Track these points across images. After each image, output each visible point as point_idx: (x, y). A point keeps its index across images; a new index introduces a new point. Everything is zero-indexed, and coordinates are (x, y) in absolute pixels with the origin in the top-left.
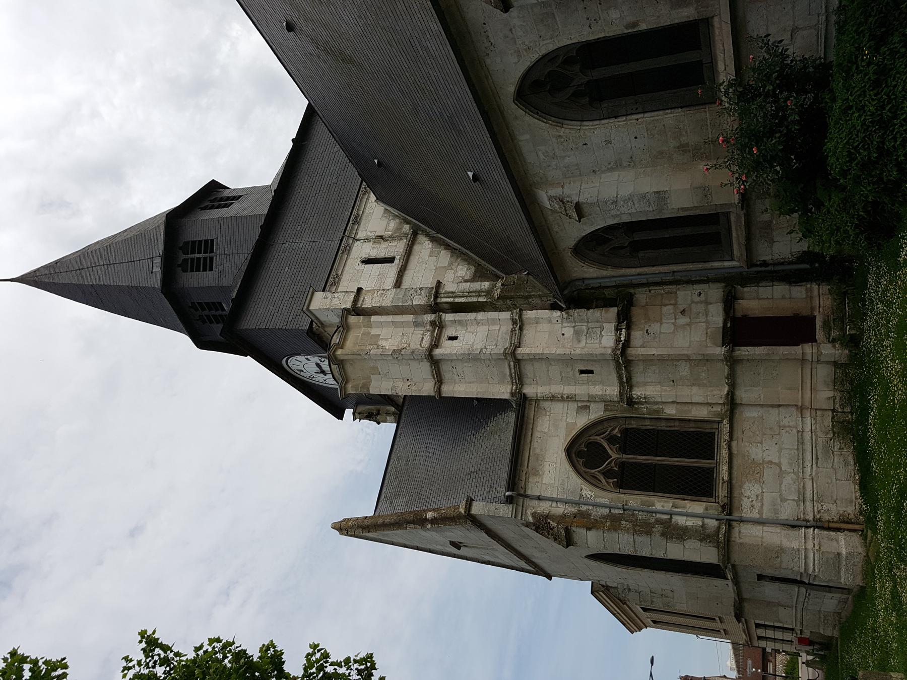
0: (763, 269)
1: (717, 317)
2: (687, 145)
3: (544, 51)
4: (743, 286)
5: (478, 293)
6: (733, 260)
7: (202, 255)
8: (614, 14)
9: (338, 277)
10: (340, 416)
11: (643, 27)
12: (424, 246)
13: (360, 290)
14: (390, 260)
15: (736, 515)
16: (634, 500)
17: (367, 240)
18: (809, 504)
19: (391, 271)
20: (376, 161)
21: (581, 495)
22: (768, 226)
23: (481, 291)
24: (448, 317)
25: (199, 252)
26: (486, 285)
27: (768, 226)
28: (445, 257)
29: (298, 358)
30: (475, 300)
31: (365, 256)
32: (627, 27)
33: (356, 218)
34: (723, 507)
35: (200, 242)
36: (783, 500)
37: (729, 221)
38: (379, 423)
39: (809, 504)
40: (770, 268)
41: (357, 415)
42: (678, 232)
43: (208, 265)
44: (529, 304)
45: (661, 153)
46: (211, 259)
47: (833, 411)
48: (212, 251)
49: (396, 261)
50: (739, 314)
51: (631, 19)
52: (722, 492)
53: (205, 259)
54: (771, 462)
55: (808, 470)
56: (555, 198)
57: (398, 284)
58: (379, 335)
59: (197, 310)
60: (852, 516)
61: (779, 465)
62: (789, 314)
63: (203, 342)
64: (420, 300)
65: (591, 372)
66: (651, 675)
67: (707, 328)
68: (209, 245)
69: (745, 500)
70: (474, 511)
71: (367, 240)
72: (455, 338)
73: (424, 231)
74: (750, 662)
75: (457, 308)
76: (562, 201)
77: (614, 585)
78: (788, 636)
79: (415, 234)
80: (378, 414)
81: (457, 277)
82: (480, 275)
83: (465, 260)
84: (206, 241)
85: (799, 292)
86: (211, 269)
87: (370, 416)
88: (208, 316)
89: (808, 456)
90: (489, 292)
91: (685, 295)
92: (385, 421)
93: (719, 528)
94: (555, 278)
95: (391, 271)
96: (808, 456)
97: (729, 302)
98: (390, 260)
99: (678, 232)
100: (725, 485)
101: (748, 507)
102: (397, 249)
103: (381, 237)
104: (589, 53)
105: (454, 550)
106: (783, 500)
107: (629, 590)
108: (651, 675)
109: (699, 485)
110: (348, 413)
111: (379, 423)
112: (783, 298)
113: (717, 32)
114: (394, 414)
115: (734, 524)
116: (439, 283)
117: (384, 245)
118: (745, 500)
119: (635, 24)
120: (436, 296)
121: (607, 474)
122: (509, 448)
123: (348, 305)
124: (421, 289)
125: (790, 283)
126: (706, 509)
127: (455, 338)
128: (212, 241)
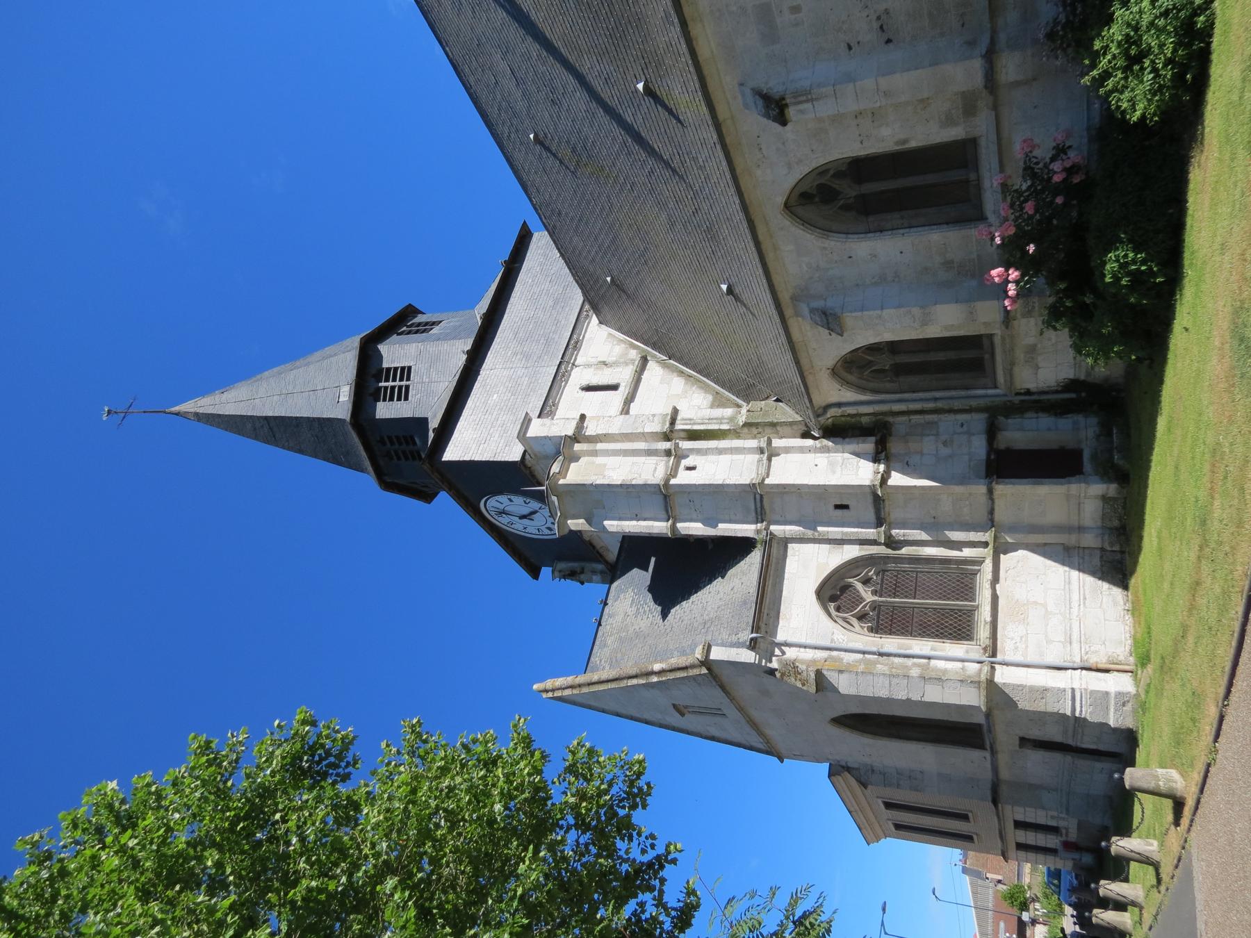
0: (1027, 398)
1: (979, 446)
2: (952, 262)
3: (814, 165)
4: (1007, 417)
5: (720, 420)
6: (996, 387)
7: (397, 383)
8: (885, 132)
9: (555, 405)
10: (535, 573)
11: (913, 144)
12: (654, 371)
13: (583, 417)
14: (614, 387)
15: (999, 658)
16: (891, 643)
17: (588, 366)
18: (1076, 646)
19: (617, 398)
20: (609, 279)
21: (832, 640)
22: (1032, 350)
23: (723, 418)
24: (686, 445)
25: (394, 380)
26: (729, 412)
27: (1032, 350)
28: (678, 383)
29: (500, 498)
30: (716, 427)
31: (585, 383)
32: (897, 143)
33: (577, 343)
34: (985, 649)
35: (396, 369)
36: (1049, 642)
37: (992, 344)
38: (582, 583)
39: (1076, 646)
40: (1035, 397)
41: (557, 574)
42: (941, 356)
43: (404, 394)
44: (777, 432)
45: (926, 269)
46: (407, 387)
47: (1102, 549)
48: (408, 379)
49: (621, 389)
50: (1002, 446)
51: (902, 136)
52: (983, 633)
53: (400, 388)
54: (1035, 603)
55: (1075, 610)
56: (817, 310)
57: (625, 410)
58: (605, 465)
59: (384, 444)
60: (1121, 658)
61: (1045, 606)
62: (1055, 446)
63: (388, 484)
64: (656, 427)
65: (837, 507)
66: (883, 924)
67: (970, 460)
68: (406, 372)
69: (1008, 641)
70: (713, 656)
71: (588, 366)
72: (693, 468)
73: (654, 356)
74: (1002, 925)
75: (693, 435)
76: (824, 313)
77: (856, 766)
78: (1052, 841)
79: (644, 360)
80: (582, 572)
81: (696, 404)
82: (719, 402)
83: (701, 388)
84: (403, 369)
85: (1065, 423)
86: (406, 398)
87: (572, 575)
88: (404, 452)
89: (1075, 597)
90: (731, 419)
91: (947, 423)
92: (590, 581)
93: (980, 670)
94: (811, 401)
95: (617, 398)
96: (1075, 597)
97: (992, 432)
98: (614, 387)
99: (941, 356)
100: (988, 627)
101: (1007, 650)
102: (623, 376)
103: (605, 363)
104: (860, 168)
105: (675, 719)
106: (1049, 642)
107: (873, 771)
108: (883, 924)
109: (956, 627)
110: (546, 572)
111: (582, 583)
112: (1049, 429)
113: (984, 151)
114: (602, 572)
115: (997, 666)
116: (675, 411)
117: (607, 371)
118: (1008, 641)
119: (905, 141)
120: (673, 422)
121: (861, 617)
122: (755, 583)
123: (570, 433)
124: (654, 415)
125: (1056, 415)
126: (967, 652)
127: (693, 468)
128: (410, 368)
